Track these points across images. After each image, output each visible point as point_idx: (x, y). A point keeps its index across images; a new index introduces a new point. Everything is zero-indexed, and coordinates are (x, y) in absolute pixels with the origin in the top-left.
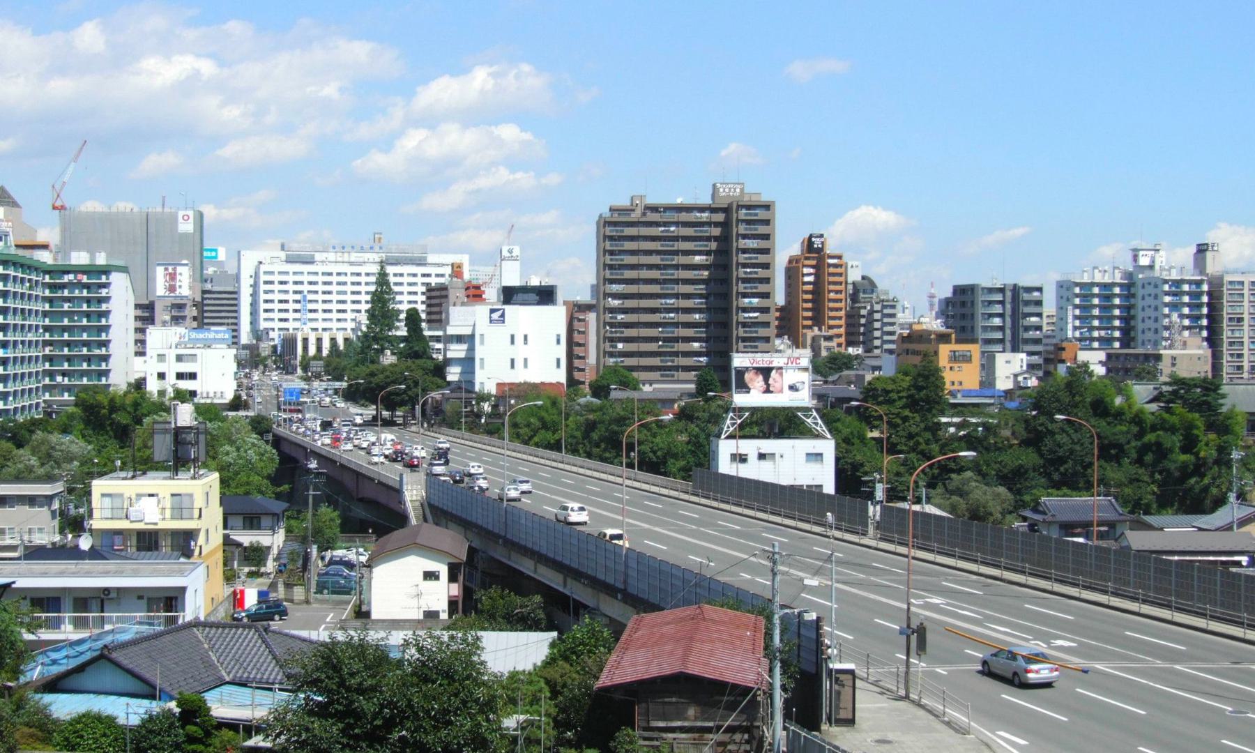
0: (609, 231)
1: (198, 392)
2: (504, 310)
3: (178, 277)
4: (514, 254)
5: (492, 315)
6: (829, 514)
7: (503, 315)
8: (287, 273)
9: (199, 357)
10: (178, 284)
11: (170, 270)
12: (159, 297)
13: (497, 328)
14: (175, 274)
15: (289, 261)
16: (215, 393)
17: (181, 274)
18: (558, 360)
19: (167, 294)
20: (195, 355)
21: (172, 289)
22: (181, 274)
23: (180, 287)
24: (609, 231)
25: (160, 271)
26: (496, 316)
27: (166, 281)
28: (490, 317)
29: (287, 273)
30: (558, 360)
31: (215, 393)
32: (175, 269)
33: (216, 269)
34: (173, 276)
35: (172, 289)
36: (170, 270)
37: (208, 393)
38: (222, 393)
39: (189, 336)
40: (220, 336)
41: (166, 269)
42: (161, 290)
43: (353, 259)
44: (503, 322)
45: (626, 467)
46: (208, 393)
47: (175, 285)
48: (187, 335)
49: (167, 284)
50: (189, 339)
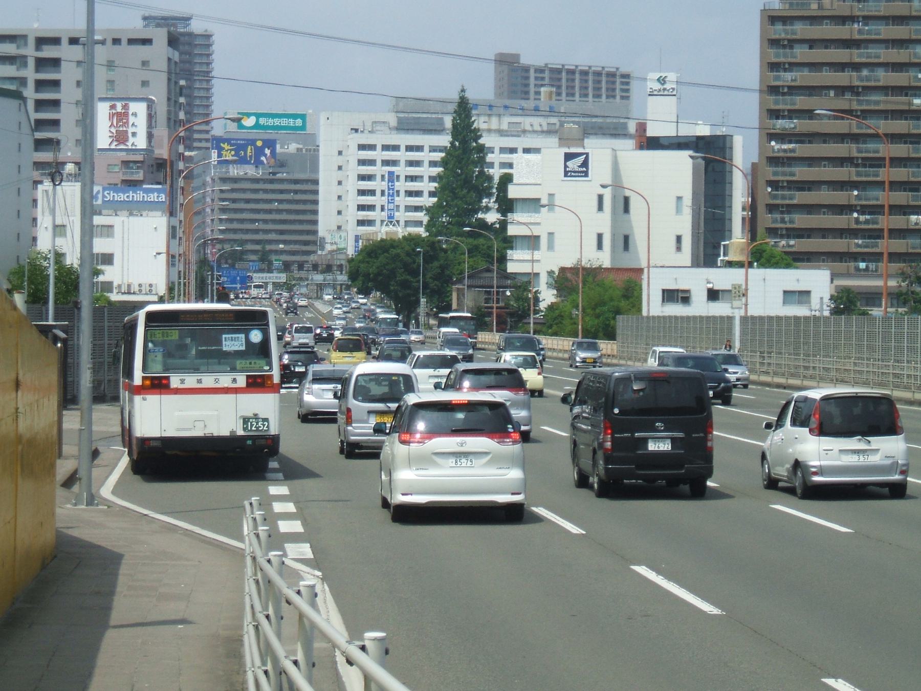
0: (779, 31)
1: (115, 284)
2: (587, 154)
3: (132, 120)
4: (668, 86)
5: (569, 163)
6: (412, 299)
7: (585, 164)
8: (396, 148)
9: (117, 230)
10: (131, 130)
11: (119, 108)
12: (100, 150)
13: (578, 185)
14: (126, 115)
15: (404, 127)
16: (140, 285)
17: (135, 114)
18: (679, 239)
19: (113, 147)
20: (111, 227)
21: (121, 137)
22: (135, 114)
23: (134, 134)
24: (779, 31)
25: (103, 110)
26: (574, 164)
27: (112, 125)
28: (566, 166)
29: (396, 148)
30: (679, 239)
31: (140, 285)
32: (125, 107)
33: (301, 146)
34: (122, 117)
35: (121, 137)
36: (119, 108)
37: (129, 286)
38: (151, 285)
39: (104, 196)
40: (153, 197)
41: (113, 107)
42: (103, 138)
43: (505, 126)
44: (586, 174)
45: (497, 332)
46: (129, 286)
47: (126, 132)
48: (100, 196)
49: (113, 130)
50: (104, 201)
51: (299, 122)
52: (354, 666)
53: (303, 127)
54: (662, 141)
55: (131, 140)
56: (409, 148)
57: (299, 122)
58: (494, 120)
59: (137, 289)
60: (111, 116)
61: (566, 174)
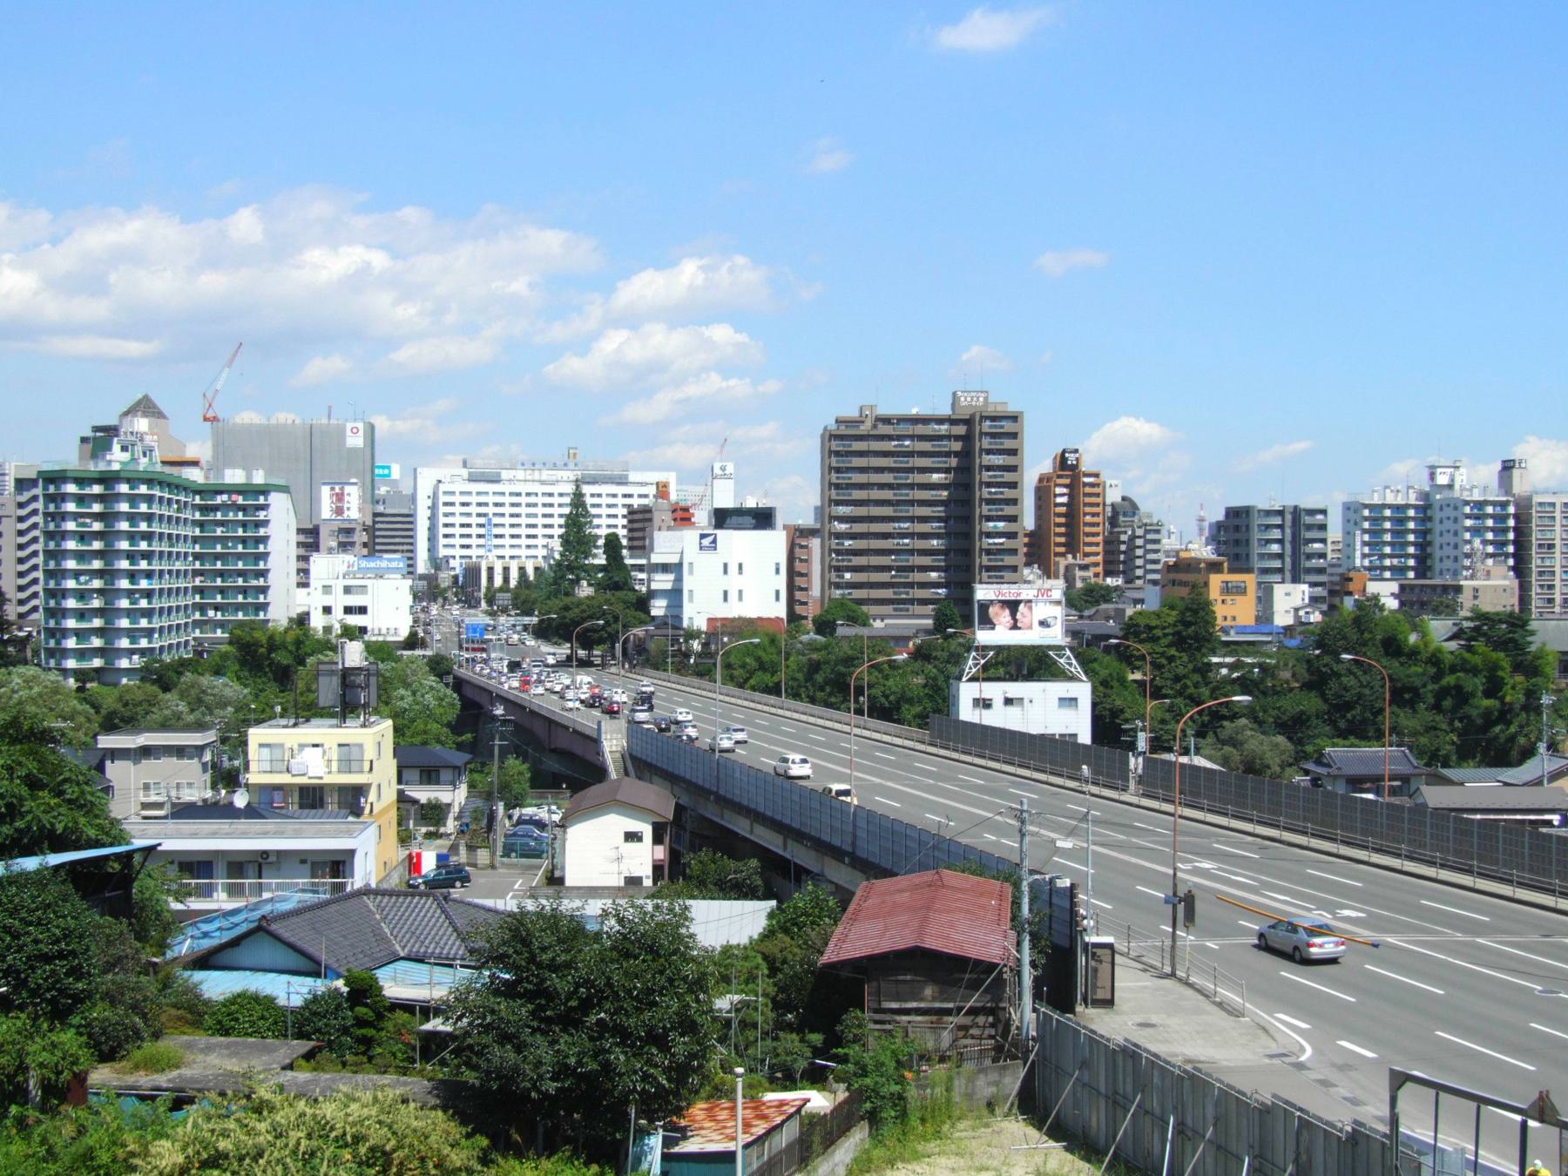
6: (1085, 767)
7: (714, 541)
8: (470, 493)
9: (370, 589)
10: (346, 506)
13: (708, 556)
14: (342, 494)
15: (473, 479)
18: (777, 593)
21: (339, 511)
24: (835, 445)
26: (706, 542)
29: (470, 493)
30: (777, 593)
32: (342, 489)
34: (340, 497)
40: (394, 564)
41: (333, 489)
44: (715, 549)
51: (386, 472)
52: (622, 884)
53: (389, 475)
54: (750, 520)
55: (346, 513)
56: (479, 493)
57: (386, 472)
58: (537, 473)
59: (384, 631)
60: (332, 496)
61: (701, 548)
